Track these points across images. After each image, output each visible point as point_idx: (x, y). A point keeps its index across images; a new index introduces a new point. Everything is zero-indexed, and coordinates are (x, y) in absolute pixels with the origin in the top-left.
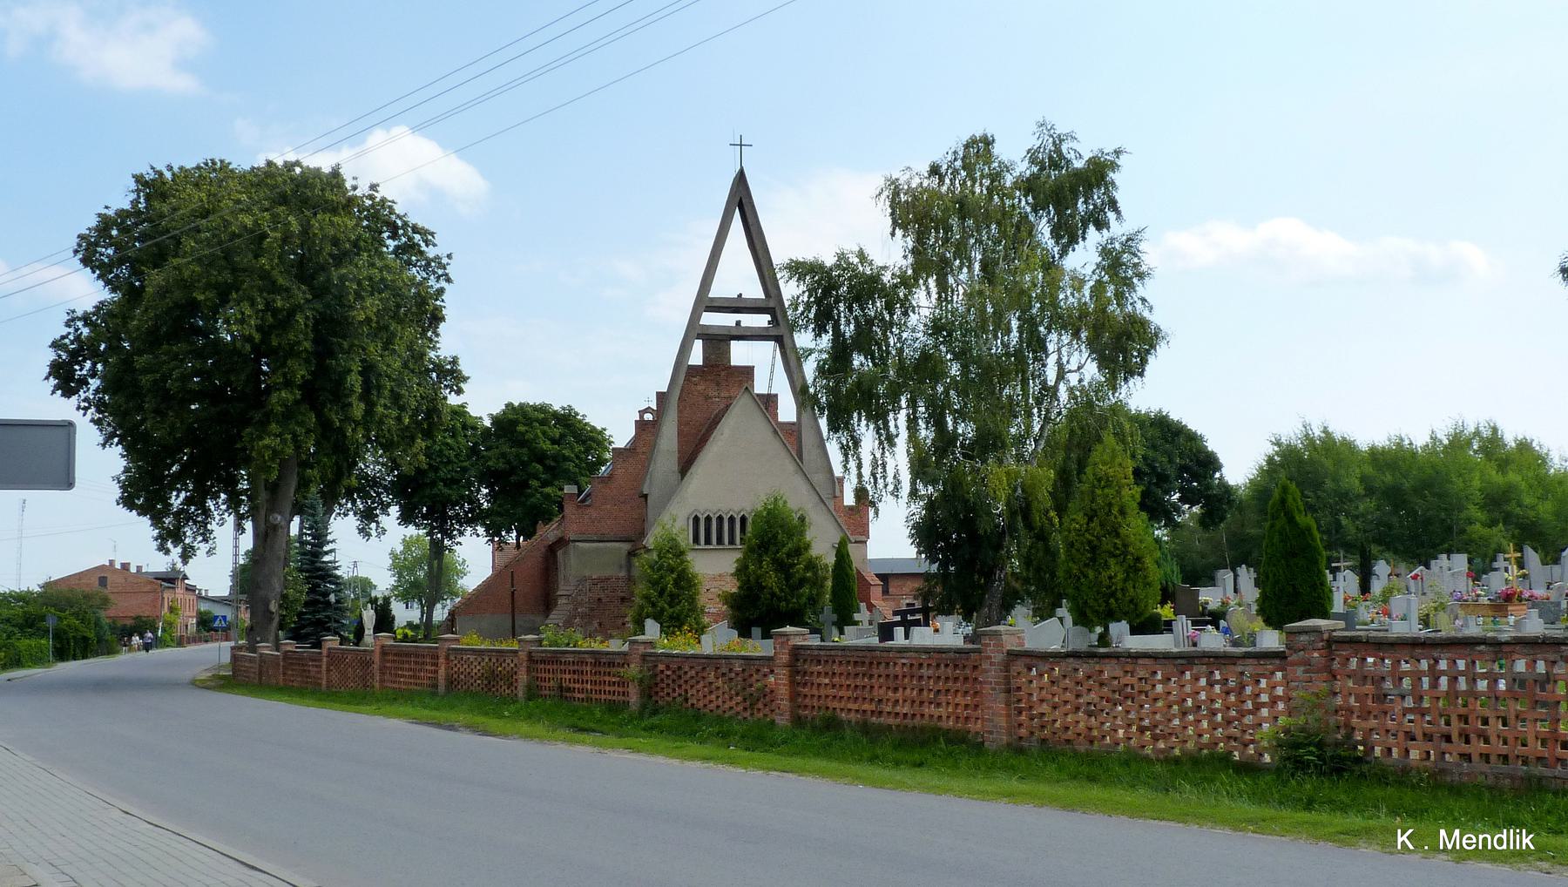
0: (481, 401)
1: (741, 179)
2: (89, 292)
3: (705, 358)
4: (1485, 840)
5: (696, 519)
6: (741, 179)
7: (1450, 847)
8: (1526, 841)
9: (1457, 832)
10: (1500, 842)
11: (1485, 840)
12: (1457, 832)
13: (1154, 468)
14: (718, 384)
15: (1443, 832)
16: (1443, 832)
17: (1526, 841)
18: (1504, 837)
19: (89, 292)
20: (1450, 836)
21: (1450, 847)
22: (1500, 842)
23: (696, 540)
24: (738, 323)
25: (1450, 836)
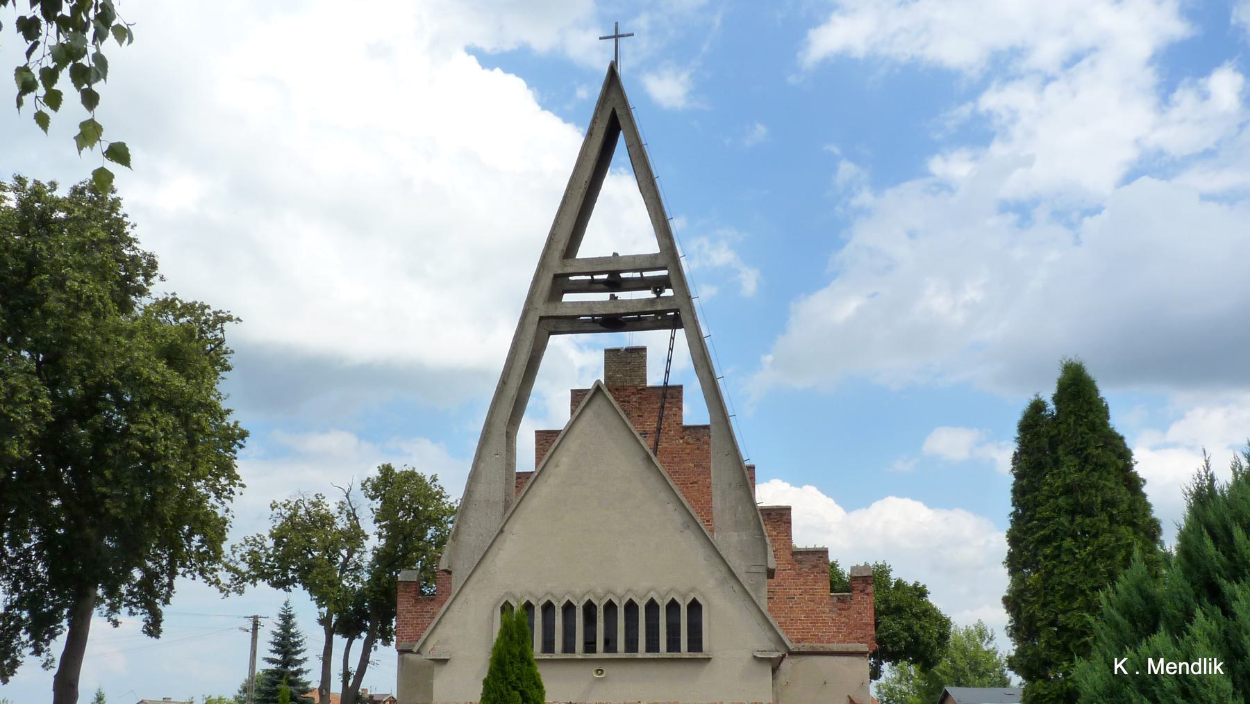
1: (613, 73)
6: (613, 73)
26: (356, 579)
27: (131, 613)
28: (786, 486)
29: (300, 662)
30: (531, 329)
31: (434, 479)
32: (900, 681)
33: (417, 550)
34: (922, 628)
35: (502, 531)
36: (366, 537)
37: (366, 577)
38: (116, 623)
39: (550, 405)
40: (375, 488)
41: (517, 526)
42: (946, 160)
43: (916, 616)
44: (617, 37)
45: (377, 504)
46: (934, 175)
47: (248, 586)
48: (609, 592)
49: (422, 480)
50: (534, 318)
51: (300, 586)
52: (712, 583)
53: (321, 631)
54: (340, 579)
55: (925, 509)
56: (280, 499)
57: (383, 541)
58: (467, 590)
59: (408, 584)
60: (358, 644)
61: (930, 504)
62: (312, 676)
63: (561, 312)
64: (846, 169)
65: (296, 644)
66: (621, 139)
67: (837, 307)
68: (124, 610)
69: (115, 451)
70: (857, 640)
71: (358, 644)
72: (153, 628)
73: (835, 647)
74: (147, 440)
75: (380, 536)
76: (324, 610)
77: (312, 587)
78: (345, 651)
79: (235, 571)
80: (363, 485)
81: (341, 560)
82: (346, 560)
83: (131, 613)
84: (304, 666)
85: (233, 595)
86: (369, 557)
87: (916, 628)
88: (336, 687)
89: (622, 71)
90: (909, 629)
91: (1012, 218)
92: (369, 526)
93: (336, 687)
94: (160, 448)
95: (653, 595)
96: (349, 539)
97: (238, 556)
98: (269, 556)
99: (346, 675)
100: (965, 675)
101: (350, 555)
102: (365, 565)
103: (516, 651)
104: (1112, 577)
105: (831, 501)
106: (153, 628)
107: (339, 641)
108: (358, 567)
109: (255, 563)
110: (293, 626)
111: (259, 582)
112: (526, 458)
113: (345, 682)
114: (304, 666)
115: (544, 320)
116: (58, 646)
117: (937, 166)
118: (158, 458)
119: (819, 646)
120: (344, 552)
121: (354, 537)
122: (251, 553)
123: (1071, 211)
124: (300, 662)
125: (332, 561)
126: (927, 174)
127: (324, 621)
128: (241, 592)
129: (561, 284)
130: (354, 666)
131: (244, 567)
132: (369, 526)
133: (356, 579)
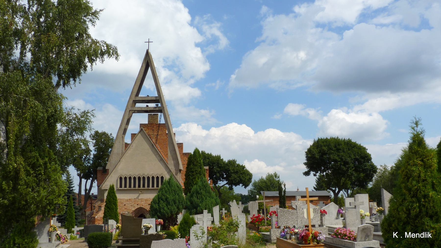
0: (227, 161)
1: (148, 53)
2: (221, 158)
3: (149, 121)
4: (418, 235)
5: (121, 178)
6: (148, 53)
7: (408, 237)
8: (429, 235)
9: (410, 233)
10: (422, 236)
11: (418, 235)
12: (410, 233)
13: (342, 159)
14: (153, 130)
15: (406, 233)
16: (406, 233)
17: (429, 235)
18: (423, 234)
19: (221, 158)
20: (408, 234)
21: (408, 237)
22: (422, 236)
23: (121, 186)
24: (147, 106)
25: (408, 234)
26: (89, 163)
28: (237, 124)
29: (73, 187)
30: (127, 113)
31: (111, 134)
32: (254, 189)
33: (106, 155)
34: (243, 177)
36: (91, 151)
37: (91, 162)
39: (134, 127)
40: (93, 137)
41: (123, 160)
42: (300, 7)
43: (242, 174)
44: (149, 42)
45: (94, 141)
46: (295, 12)
48: (144, 174)
49: (107, 134)
50: (128, 110)
51: (72, 165)
53: (78, 178)
54: (83, 163)
55: (281, 132)
57: (96, 152)
58: (112, 174)
59: (100, 170)
60: (89, 181)
61: (283, 130)
62: (76, 191)
63: (134, 109)
64: (264, 9)
65: (72, 182)
66: (149, 70)
67: (259, 58)
71: (89, 181)
75: (95, 151)
76: (79, 172)
77: (75, 166)
78: (86, 183)
80: (90, 136)
81: (84, 157)
82: (85, 157)
84: (74, 188)
86: (92, 156)
87: (241, 177)
88: (83, 193)
89: (150, 51)
90: (239, 177)
91: (320, 29)
92: (92, 148)
93: (83, 193)
95: (153, 175)
96: (86, 152)
99: (86, 190)
100: (269, 188)
101: (86, 156)
102: (91, 159)
103: (112, 191)
105: (250, 128)
107: (84, 181)
108: (89, 159)
110: (70, 177)
112: (128, 139)
113: (86, 192)
114: (74, 188)
115: (131, 111)
117: (296, 9)
120: (85, 156)
121: (88, 151)
123: (340, 29)
124: (73, 187)
125: (81, 158)
126: (293, 12)
127: (79, 175)
129: (135, 102)
130: (88, 187)
132: (92, 148)
133: (89, 163)
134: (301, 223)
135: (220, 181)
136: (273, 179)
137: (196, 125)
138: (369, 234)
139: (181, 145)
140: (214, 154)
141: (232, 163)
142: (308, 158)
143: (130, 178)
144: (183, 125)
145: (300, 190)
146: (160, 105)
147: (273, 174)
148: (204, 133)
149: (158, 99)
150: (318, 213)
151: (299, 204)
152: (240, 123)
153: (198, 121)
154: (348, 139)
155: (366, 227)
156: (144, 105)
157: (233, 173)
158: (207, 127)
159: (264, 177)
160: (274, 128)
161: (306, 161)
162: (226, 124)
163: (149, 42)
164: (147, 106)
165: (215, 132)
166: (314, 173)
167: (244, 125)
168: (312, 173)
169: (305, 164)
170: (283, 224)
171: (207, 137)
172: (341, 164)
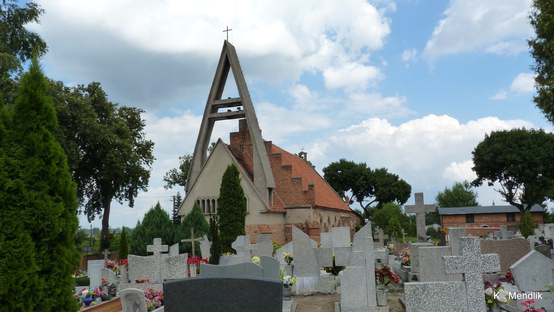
2: (367, 167)
3: (240, 129)
13: (524, 158)
19: (367, 167)
27: (126, 200)
28: (435, 116)
35: (196, 180)
38: (122, 203)
41: (200, 179)
44: (227, 31)
47: (173, 186)
50: (207, 118)
52: (249, 192)
56: (182, 156)
68: (124, 199)
69: (23, 239)
70: (309, 203)
72: (131, 205)
73: (303, 206)
74: (111, 158)
79: (168, 181)
83: (126, 200)
85: (169, 189)
90: (390, 191)
94: (114, 160)
97: (169, 176)
98: (178, 176)
104: (234, 206)
106: (131, 205)
109: (175, 178)
111: (176, 184)
116: (103, 212)
118: (114, 163)
119: (298, 205)
122: (173, 175)
128: (171, 188)
131: (171, 180)
134: (160, 276)
135: (368, 196)
136: (463, 189)
137: (379, 120)
138: (138, 302)
139: (278, 156)
140: (357, 162)
141: (382, 173)
142: (476, 161)
143: (208, 201)
144: (364, 122)
145: (496, 205)
146: (242, 108)
147: (462, 183)
148: (392, 130)
149: (240, 100)
150: (183, 262)
151: (156, 249)
152: (439, 114)
153: (381, 115)
154: (538, 129)
155: (135, 292)
156: (225, 110)
157: (381, 186)
158: (396, 122)
159: (451, 188)
160: (493, 116)
161: (474, 166)
162: (420, 117)
163: (227, 31)
164: (229, 111)
165: (407, 127)
166: (490, 181)
167: (446, 116)
168: (486, 182)
169: (473, 169)
170: (134, 277)
171: (394, 136)
172: (524, 168)
